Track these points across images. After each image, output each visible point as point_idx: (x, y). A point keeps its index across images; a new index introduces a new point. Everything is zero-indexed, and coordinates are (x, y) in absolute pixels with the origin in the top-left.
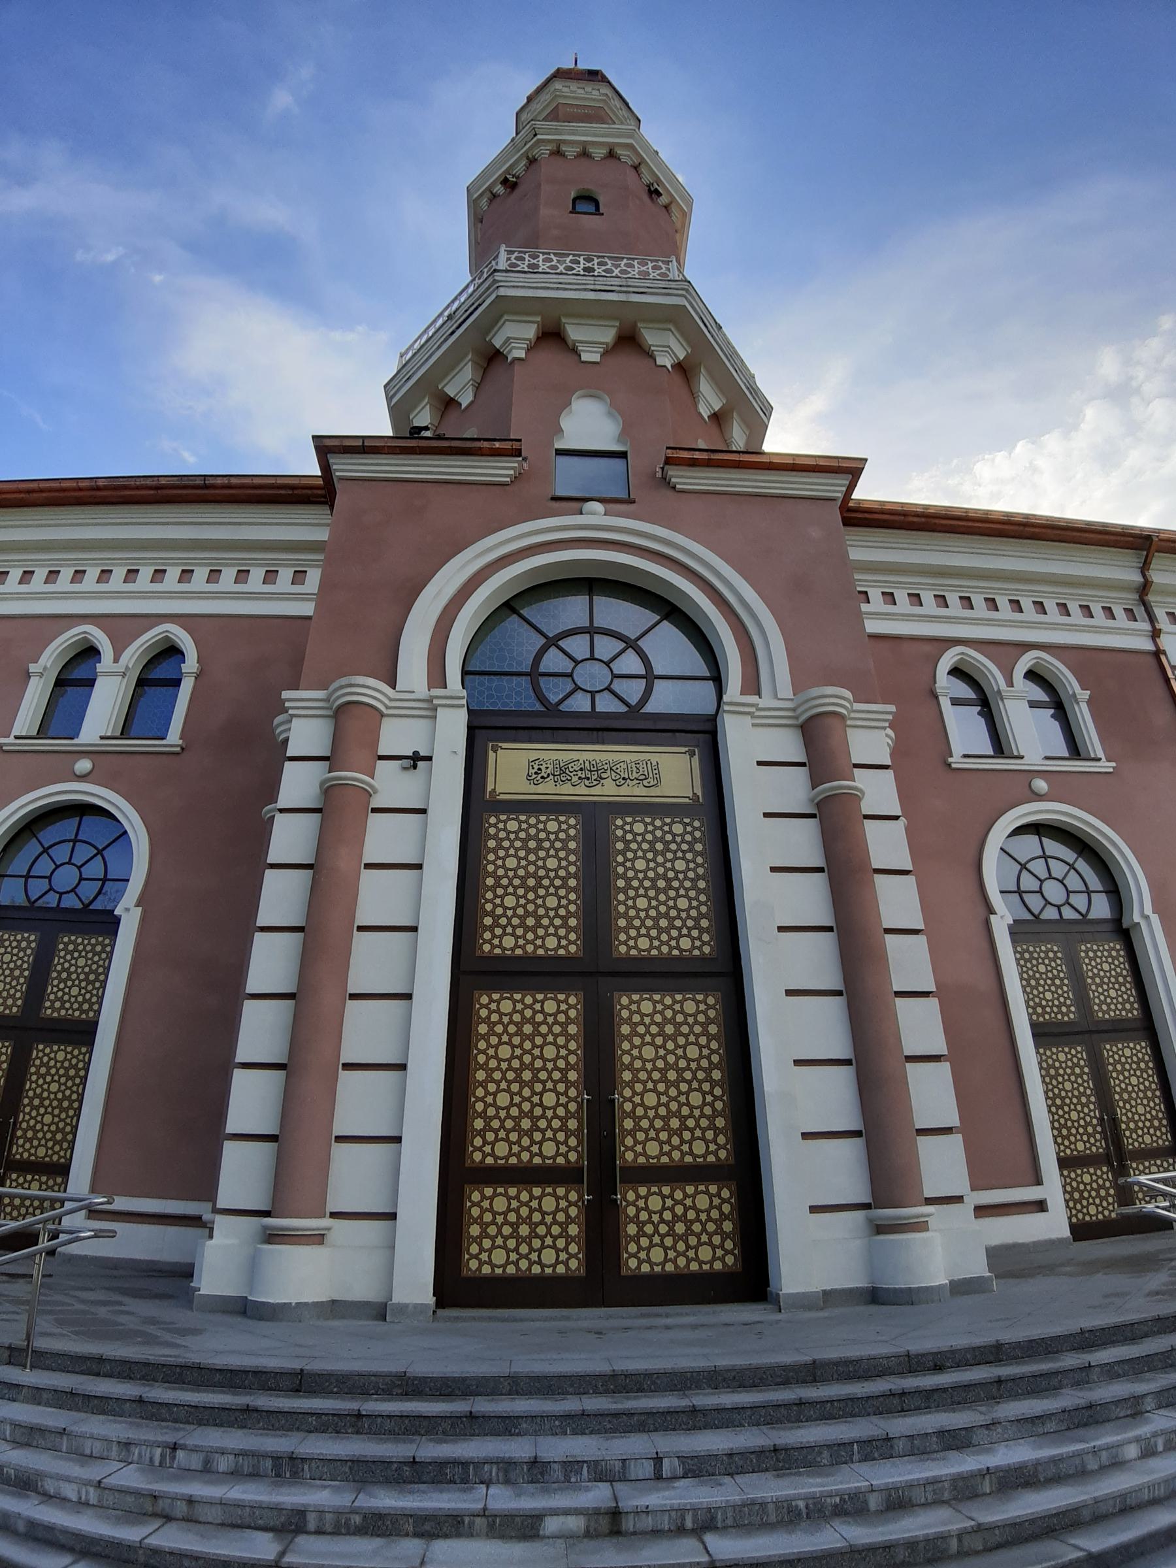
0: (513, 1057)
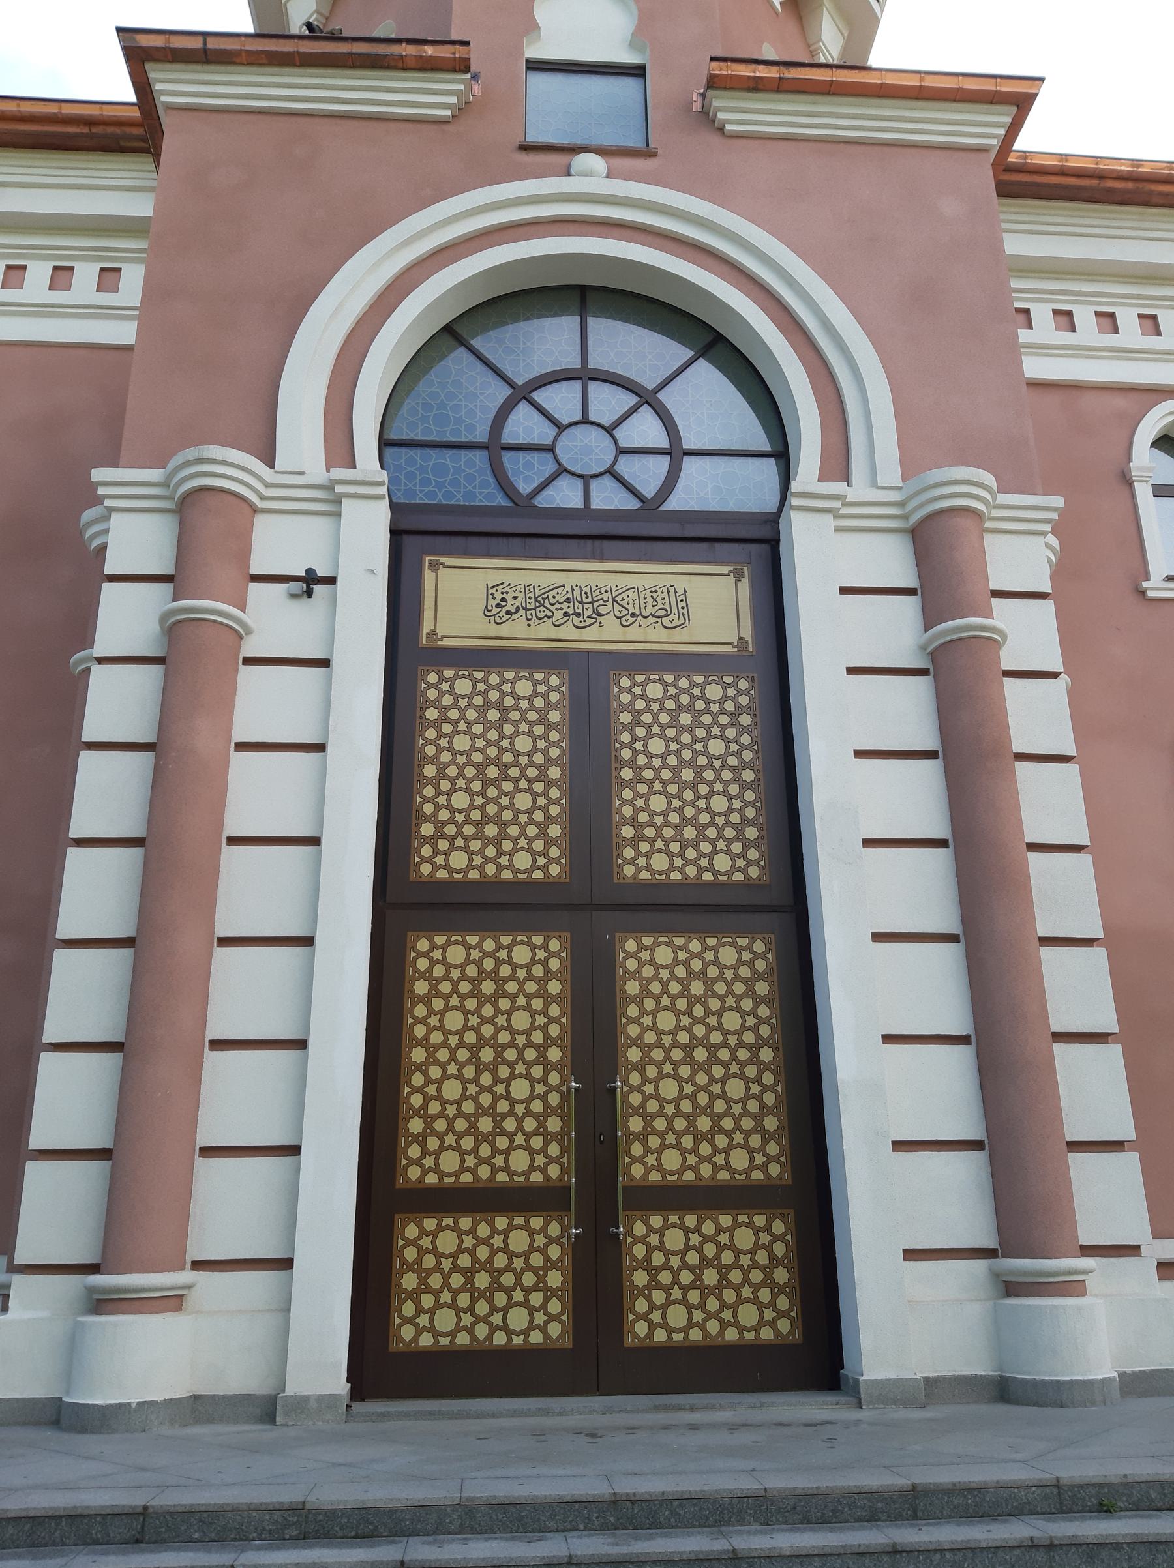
0: (466, 1028)
